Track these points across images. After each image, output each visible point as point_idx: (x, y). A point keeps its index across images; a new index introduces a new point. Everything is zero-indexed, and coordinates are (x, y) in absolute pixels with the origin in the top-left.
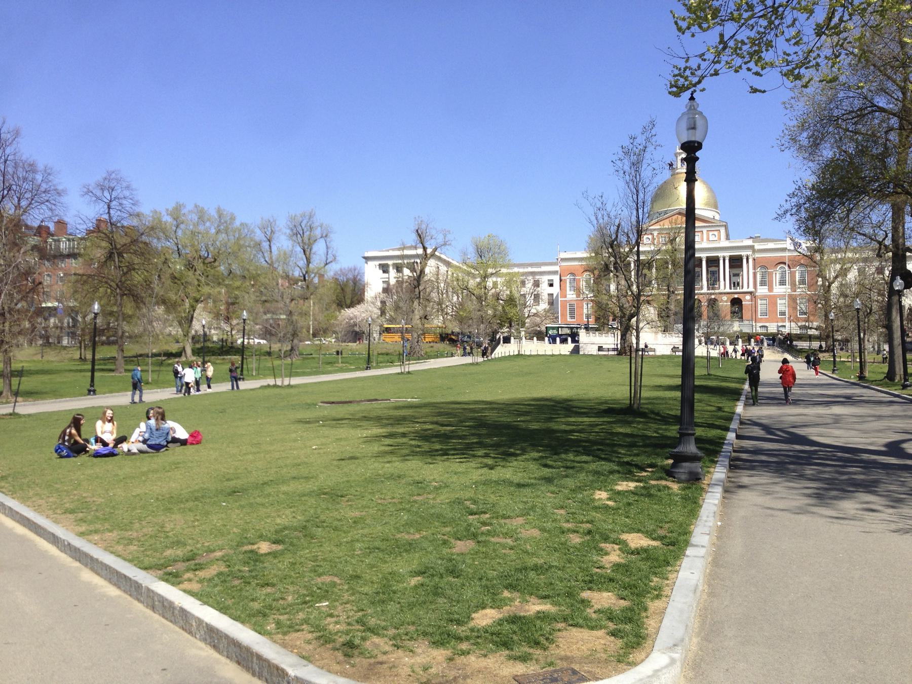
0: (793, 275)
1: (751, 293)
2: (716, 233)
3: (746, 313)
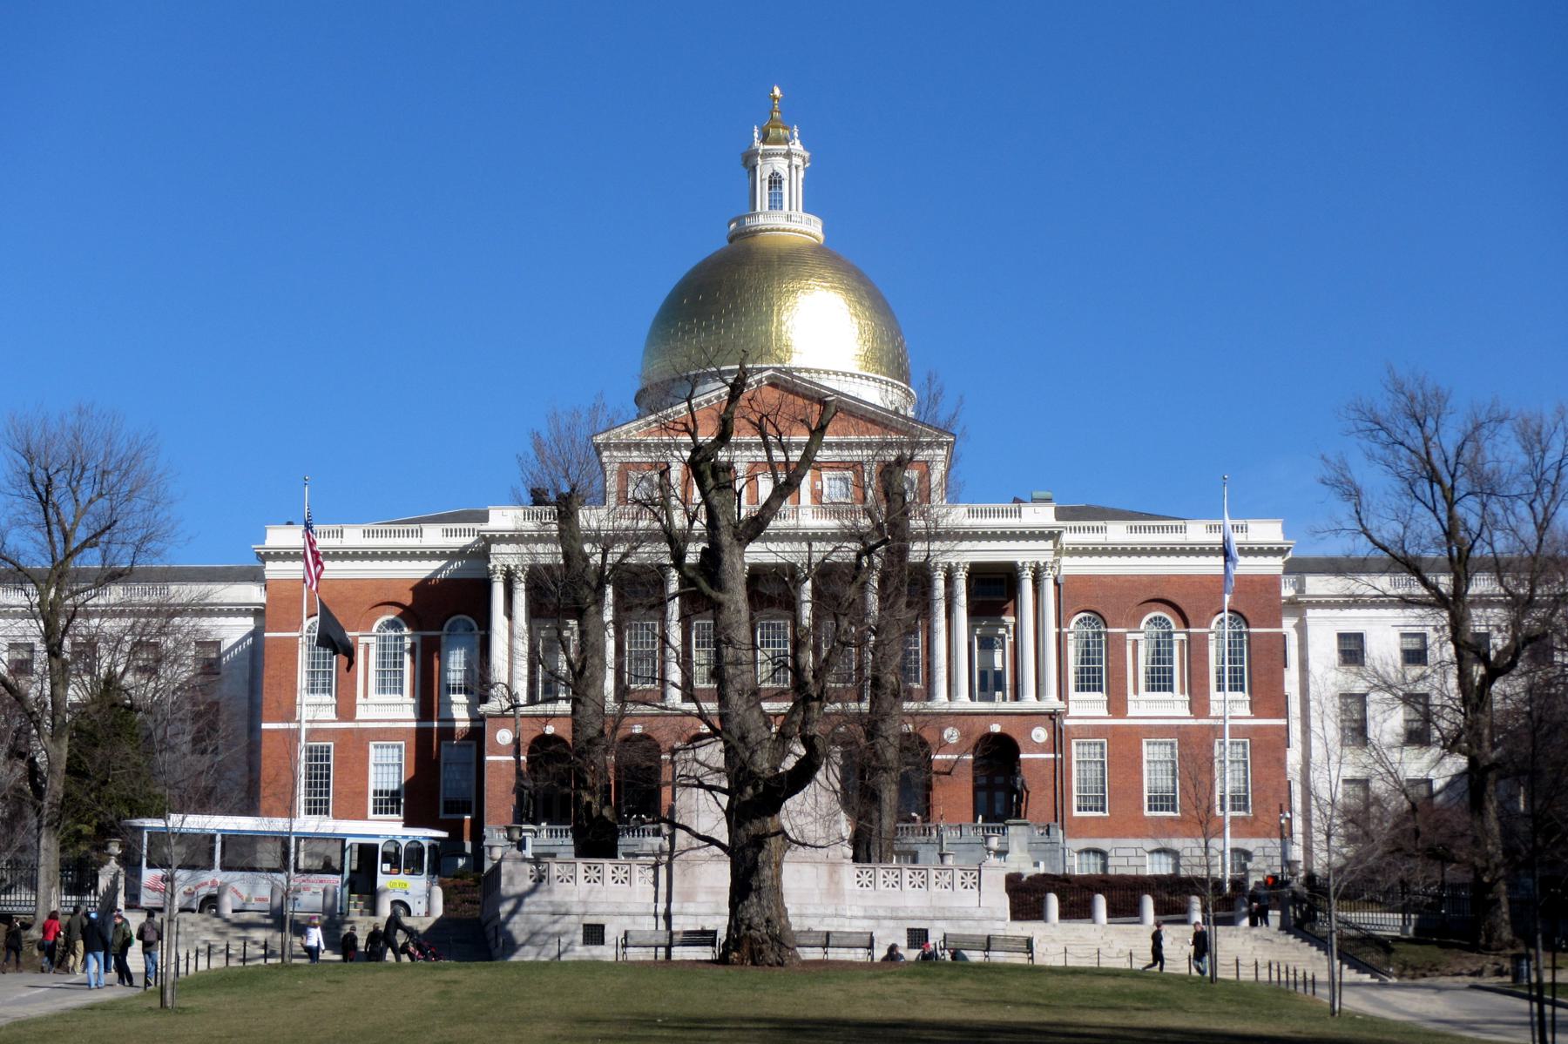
0: (1196, 650)
1: (1053, 716)
3: (1038, 802)
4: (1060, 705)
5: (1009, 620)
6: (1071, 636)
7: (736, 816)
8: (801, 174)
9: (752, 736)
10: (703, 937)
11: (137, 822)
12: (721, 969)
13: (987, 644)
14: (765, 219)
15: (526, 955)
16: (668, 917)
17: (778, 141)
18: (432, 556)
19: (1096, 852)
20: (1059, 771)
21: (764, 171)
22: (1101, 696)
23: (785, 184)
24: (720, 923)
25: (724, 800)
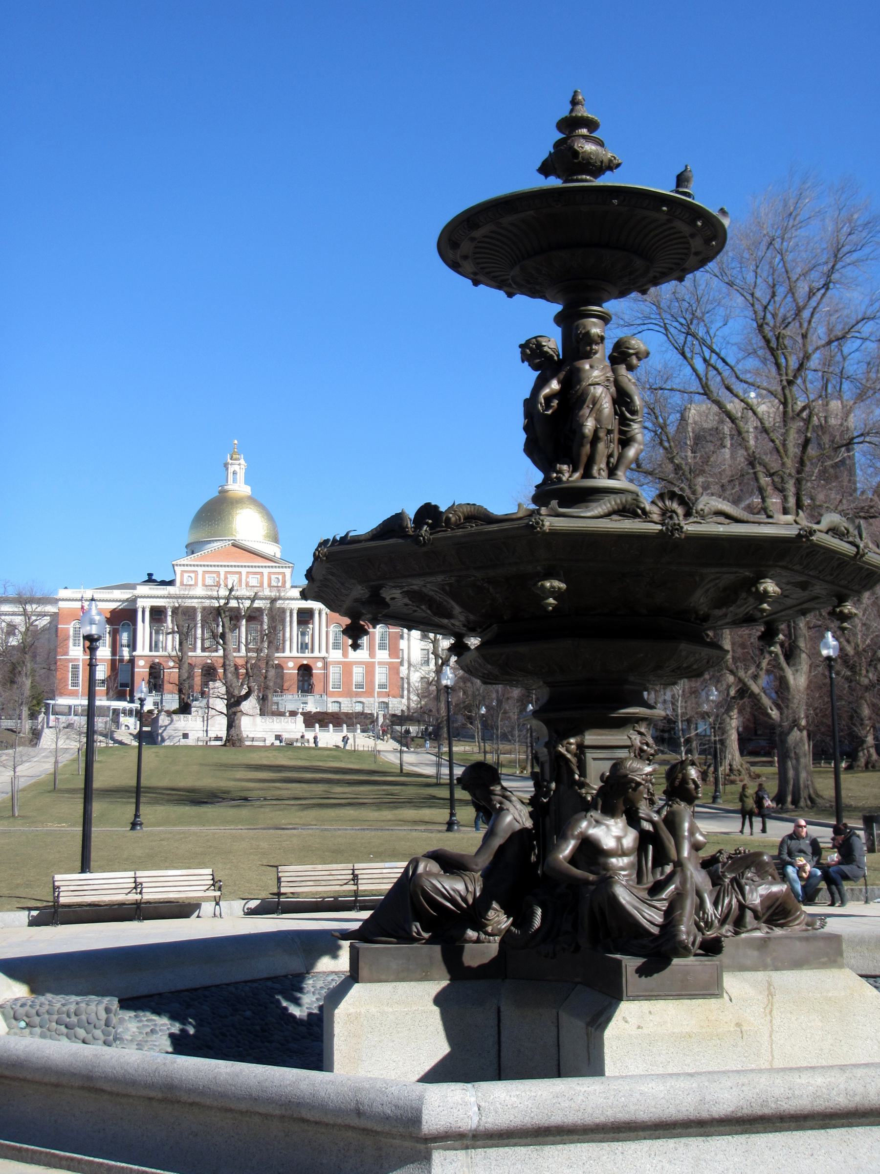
2: (193, 575)
3: (318, 686)
4: (326, 655)
5: (311, 626)
6: (331, 632)
7: (228, 706)
8: (244, 470)
9: (234, 685)
10: (217, 739)
11: (49, 702)
12: (224, 748)
13: (303, 634)
14: (231, 486)
15: (167, 743)
16: (207, 731)
17: (236, 459)
18: (117, 601)
19: (337, 702)
20: (326, 676)
21: (231, 469)
22: (340, 651)
23: (238, 474)
24: (223, 734)
25: (226, 702)
